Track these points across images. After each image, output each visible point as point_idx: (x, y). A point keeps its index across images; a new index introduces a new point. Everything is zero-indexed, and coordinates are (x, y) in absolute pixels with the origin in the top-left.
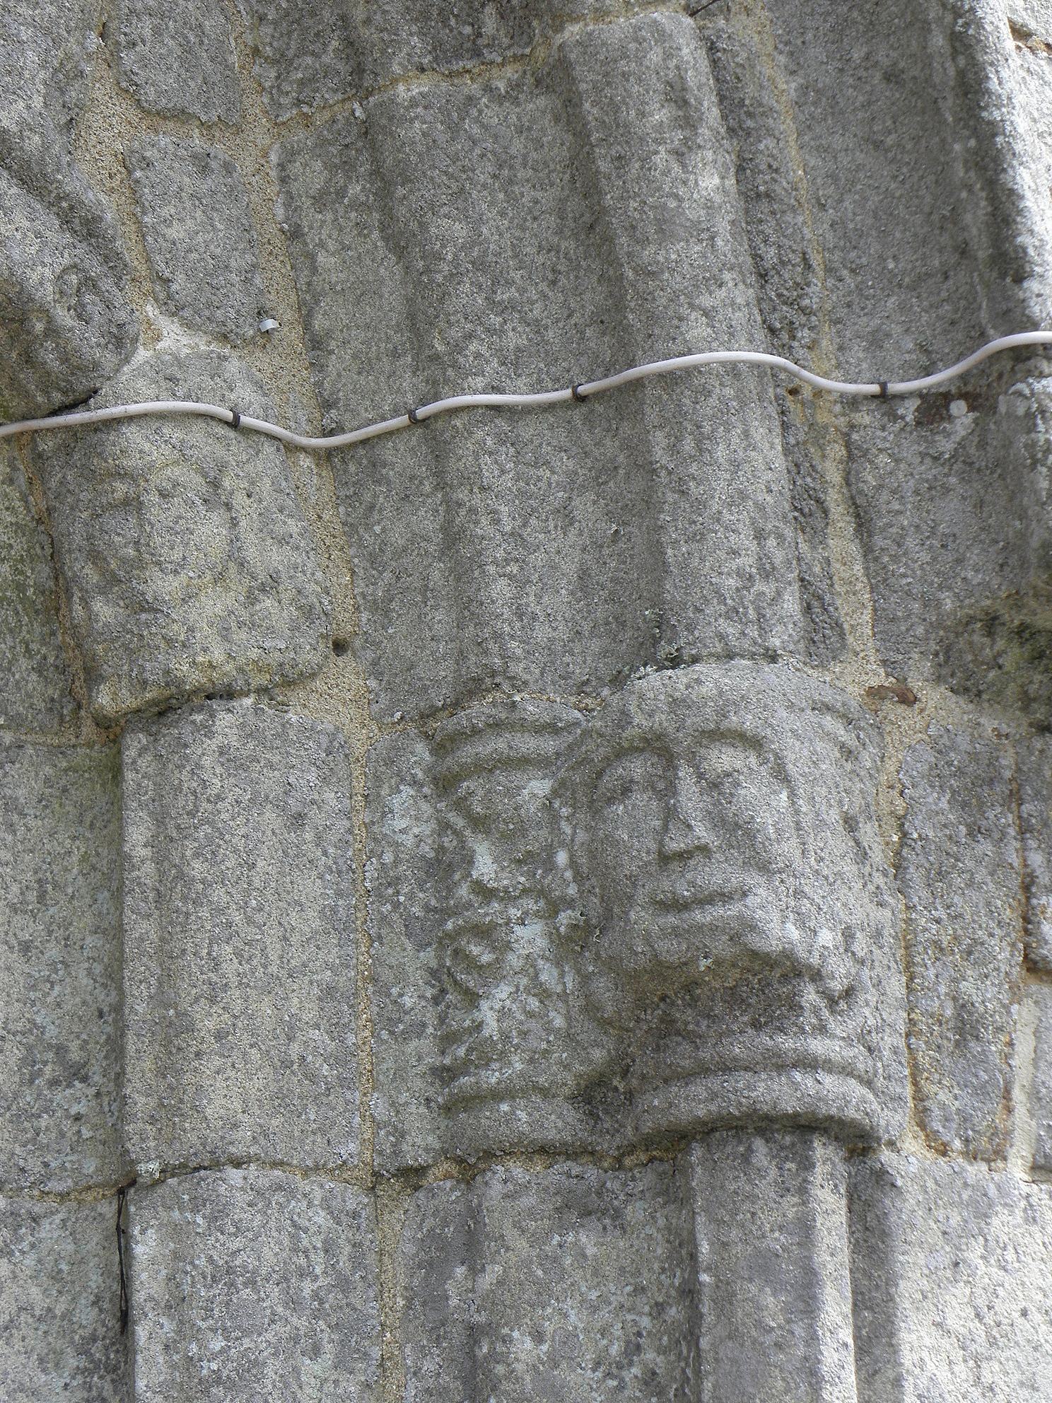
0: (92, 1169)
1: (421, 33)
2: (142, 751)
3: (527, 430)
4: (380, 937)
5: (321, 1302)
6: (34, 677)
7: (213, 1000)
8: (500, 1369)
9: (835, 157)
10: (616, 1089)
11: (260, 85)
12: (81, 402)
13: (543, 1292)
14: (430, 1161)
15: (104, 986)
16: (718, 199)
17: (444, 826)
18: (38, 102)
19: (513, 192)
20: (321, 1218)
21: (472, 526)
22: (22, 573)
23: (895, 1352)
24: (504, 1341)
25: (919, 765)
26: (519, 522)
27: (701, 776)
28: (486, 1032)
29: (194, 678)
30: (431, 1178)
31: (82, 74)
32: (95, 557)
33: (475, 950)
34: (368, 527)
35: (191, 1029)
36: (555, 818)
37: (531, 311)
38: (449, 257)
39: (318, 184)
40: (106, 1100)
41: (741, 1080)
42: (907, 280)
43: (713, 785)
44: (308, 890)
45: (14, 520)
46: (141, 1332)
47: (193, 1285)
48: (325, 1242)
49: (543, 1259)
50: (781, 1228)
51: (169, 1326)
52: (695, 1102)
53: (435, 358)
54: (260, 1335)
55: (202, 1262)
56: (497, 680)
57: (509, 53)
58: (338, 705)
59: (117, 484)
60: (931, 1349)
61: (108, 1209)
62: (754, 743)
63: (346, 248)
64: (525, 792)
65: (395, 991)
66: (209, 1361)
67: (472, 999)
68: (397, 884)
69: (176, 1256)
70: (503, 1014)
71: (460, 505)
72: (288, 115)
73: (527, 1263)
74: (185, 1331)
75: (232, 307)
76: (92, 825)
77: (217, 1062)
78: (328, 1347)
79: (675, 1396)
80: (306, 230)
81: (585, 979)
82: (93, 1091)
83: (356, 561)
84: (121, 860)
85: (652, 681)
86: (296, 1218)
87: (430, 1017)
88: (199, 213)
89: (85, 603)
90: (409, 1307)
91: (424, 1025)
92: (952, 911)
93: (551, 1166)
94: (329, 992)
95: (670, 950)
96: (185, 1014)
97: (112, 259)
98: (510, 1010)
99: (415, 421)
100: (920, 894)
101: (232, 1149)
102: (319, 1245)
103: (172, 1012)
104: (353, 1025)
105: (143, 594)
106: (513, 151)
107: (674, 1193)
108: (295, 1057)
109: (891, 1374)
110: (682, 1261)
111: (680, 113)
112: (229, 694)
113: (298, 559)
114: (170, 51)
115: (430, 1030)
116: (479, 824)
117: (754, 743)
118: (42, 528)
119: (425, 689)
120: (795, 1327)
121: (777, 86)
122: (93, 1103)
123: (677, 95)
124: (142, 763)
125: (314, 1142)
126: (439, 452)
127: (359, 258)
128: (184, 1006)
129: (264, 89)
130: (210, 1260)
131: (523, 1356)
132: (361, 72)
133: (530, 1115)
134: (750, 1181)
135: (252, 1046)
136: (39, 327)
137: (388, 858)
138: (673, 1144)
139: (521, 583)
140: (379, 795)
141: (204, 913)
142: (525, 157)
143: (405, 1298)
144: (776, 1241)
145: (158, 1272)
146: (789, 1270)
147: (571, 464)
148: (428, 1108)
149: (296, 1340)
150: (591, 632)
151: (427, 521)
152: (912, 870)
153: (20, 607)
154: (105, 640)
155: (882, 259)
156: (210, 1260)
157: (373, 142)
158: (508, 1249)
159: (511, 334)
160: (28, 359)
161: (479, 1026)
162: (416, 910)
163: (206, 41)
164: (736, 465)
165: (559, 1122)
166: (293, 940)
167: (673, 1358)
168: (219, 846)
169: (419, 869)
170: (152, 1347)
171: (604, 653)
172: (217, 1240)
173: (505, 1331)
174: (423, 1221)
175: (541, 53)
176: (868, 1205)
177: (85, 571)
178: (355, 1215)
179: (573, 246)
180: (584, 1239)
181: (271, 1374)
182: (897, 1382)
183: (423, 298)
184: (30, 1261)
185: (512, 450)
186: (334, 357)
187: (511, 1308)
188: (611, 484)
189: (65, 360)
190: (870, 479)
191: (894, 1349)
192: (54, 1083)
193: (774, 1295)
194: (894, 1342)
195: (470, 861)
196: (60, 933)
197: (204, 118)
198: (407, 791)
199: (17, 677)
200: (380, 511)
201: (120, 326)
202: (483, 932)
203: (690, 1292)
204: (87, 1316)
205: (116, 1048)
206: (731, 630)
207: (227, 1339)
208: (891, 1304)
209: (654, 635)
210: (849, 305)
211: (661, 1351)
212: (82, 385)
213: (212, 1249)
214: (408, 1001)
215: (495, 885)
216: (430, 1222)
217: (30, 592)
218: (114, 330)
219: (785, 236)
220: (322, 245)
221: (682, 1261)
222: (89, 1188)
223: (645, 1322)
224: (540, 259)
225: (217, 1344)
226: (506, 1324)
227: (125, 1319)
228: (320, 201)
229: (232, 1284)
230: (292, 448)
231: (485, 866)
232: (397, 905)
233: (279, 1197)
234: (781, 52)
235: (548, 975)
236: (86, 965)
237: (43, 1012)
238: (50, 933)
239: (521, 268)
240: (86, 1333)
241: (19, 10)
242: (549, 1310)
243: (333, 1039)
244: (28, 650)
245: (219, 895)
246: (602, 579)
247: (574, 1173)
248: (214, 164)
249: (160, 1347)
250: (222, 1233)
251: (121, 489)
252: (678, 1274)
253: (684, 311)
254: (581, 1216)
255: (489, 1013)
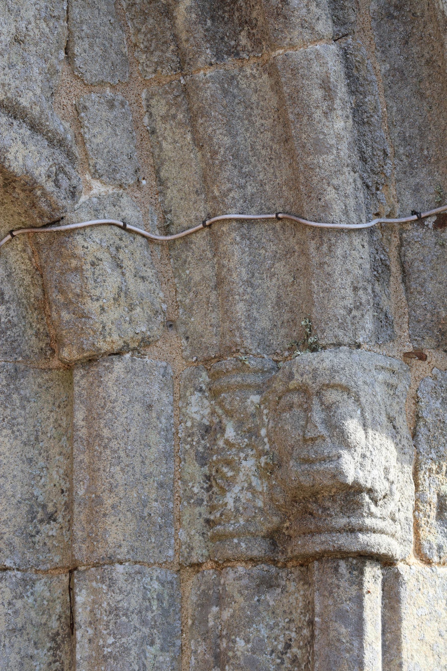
0: (58, 560)
1: (211, 47)
2: (83, 376)
3: (255, 232)
4: (185, 459)
5: (155, 622)
6: (34, 338)
7: (111, 491)
8: (230, 654)
9: (402, 101)
10: (284, 533)
11: (138, 61)
12: (57, 222)
13: (250, 621)
14: (204, 561)
15: (64, 479)
16: (343, 133)
17: (213, 413)
18: (38, 91)
19: (252, 120)
20: (156, 585)
21: (229, 277)
22: (29, 291)
23: (400, 652)
24: (233, 642)
25: (426, 388)
26: (250, 275)
27: (322, 404)
28: (229, 507)
29: (105, 347)
30: (204, 568)
31: (57, 72)
32: (61, 291)
33: (225, 470)
34: (184, 271)
35: (101, 503)
36: (260, 413)
37: (259, 176)
38: (222, 153)
39: (163, 112)
40: (64, 530)
41: (335, 536)
42: (432, 160)
43: (328, 408)
44: (153, 440)
45: (25, 268)
46: (78, 634)
47: (101, 614)
48: (158, 595)
49: (251, 606)
50: (350, 599)
51: (91, 631)
52: (316, 544)
53: (214, 198)
54: (129, 636)
55: (105, 605)
56: (239, 348)
57: (252, 55)
58: (169, 355)
59: (73, 261)
60: (417, 651)
61: (65, 579)
62: (346, 389)
63: (175, 142)
64: (249, 400)
65: (190, 484)
66: (107, 648)
67: (223, 491)
68: (192, 436)
69: (94, 602)
70: (237, 500)
71: (223, 266)
72: (150, 77)
73: (243, 609)
74: (97, 634)
75: (124, 172)
76: (59, 406)
77: (113, 518)
78: (158, 641)
79: (305, 668)
80: (158, 131)
81: (271, 488)
82: (58, 526)
83: (178, 285)
84: (72, 426)
85: (304, 357)
86: (145, 586)
87: (205, 496)
88: (110, 129)
89: (58, 313)
90: (193, 624)
91: (202, 500)
92: (439, 454)
93: (255, 566)
94: (161, 485)
95: (306, 482)
96: (99, 497)
97: (69, 155)
98: (239, 497)
99: (205, 226)
100: (423, 447)
101: (119, 557)
102: (155, 597)
103: (93, 496)
104: (172, 499)
105: (83, 310)
106: (252, 101)
107: (306, 580)
108: (146, 514)
109: (398, 662)
110: (309, 610)
111: (327, 94)
112: (119, 354)
113: (152, 287)
114: (97, 54)
115: (205, 503)
116: (229, 414)
117: (346, 389)
118: (38, 273)
119: (207, 348)
120: (354, 642)
121: (376, 69)
122: (59, 531)
123: (327, 87)
124: (82, 382)
125: (153, 552)
126: (215, 242)
127: (182, 147)
128: (99, 493)
129: (139, 63)
130: (108, 604)
131: (240, 649)
132: (183, 64)
133: (246, 544)
134: (337, 579)
135: (127, 511)
136: (39, 193)
137: (189, 424)
138: (305, 562)
139: (250, 303)
140: (185, 395)
141: (108, 452)
142: (258, 103)
143: (192, 619)
144: (348, 606)
145: (86, 608)
146: (353, 618)
147: (274, 247)
148: (204, 537)
149: (144, 638)
150: (281, 325)
151: (209, 271)
152: (420, 436)
153: (28, 307)
154: (66, 329)
155: (422, 150)
156: (108, 604)
157: (188, 95)
158: (235, 602)
159: (249, 187)
160: (33, 205)
161: (226, 504)
162: (201, 449)
163: (113, 45)
164: (345, 257)
165: (258, 549)
166: (147, 462)
167: (304, 651)
168: (115, 423)
169: (202, 430)
170: (83, 640)
171: (287, 336)
172: (112, 596)
173: (233, 637)
174: (200, 586)
175: (266, 57)
176: (391, 588)
177: (58, 297)
178: (172, 583)
179: (278, 147)
180: (268, 598)
181: (133, 653)
182: (400, 665)
183: (210, 170)
184: (31, 600)
185: (248, 242)
186: (169, 190)
187: (236, 627)
188: (292, 259)
189: (50, 206)
190: (410, 255)
191: (399, 650)
192: (41, 521)
193: (346, 628)
194: (399, 648)
195: (223, 430)
196: (45, 454)
197: (112, 83)
198: (198, 394)
199: (26, 338)
200: (189, 264)
201: (74, 188)
202: (228, 463)
203: (311, 623)
204: (55, 624)
205: (68, 506)
206: (340, 333)
207: (115, 638)
208: (399, 632)
209: (306, 333)
210: (405, 173)
211: (300, 648)
212: (57, 215)
213: (109, 599)
214: (196, 490)
215: (234, 442)
216: (202, 587)
217: (32, 300)
218: (72, 189)
219: (375, 142)
220: (165, 138)
221: (309, 610)
222: (57, 568)
223: (293, 635)
224: (264, 152)
225: (111, 640)
226: (234, 634)
227: (72, 626)
228: (164, 118)
229: (117, 615)
230: (150, 240)
231: (230, 433)
232: (192, 446)
233: (139, 576)
234: (378, 51)
235: (255, 482)
236: (56, 469)
237: (37, 489)
238: (40, 454)
239: (255, 156)
240: (54, 631)
241: (30, 49)
242: (252, 629)
243: (163, 506)
244: (31, 326)
245: (114, 444)
246: (287, 302)
247: (265, 569)
248: (116, 103)
249: (86, 641)
250: (114, 593)
251: (74, 263)
252: (308, 615)
253: (326, 186)
254: (267, 588)
255: (230, 499)
